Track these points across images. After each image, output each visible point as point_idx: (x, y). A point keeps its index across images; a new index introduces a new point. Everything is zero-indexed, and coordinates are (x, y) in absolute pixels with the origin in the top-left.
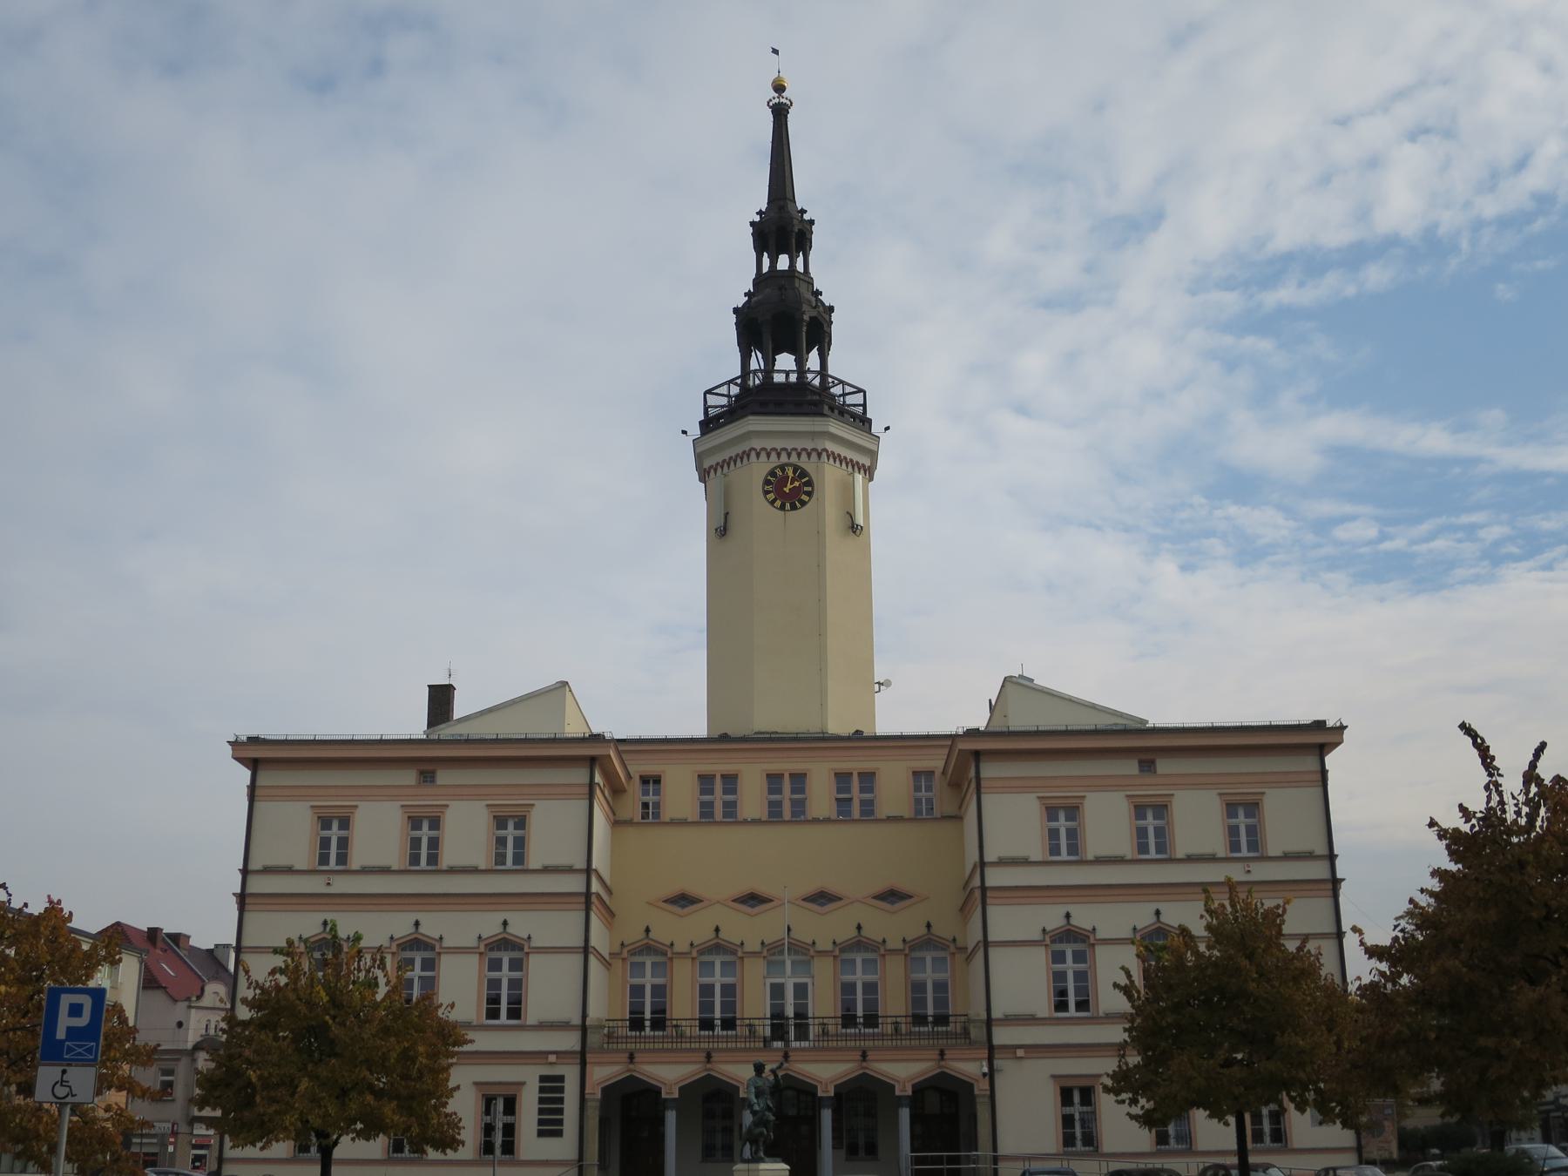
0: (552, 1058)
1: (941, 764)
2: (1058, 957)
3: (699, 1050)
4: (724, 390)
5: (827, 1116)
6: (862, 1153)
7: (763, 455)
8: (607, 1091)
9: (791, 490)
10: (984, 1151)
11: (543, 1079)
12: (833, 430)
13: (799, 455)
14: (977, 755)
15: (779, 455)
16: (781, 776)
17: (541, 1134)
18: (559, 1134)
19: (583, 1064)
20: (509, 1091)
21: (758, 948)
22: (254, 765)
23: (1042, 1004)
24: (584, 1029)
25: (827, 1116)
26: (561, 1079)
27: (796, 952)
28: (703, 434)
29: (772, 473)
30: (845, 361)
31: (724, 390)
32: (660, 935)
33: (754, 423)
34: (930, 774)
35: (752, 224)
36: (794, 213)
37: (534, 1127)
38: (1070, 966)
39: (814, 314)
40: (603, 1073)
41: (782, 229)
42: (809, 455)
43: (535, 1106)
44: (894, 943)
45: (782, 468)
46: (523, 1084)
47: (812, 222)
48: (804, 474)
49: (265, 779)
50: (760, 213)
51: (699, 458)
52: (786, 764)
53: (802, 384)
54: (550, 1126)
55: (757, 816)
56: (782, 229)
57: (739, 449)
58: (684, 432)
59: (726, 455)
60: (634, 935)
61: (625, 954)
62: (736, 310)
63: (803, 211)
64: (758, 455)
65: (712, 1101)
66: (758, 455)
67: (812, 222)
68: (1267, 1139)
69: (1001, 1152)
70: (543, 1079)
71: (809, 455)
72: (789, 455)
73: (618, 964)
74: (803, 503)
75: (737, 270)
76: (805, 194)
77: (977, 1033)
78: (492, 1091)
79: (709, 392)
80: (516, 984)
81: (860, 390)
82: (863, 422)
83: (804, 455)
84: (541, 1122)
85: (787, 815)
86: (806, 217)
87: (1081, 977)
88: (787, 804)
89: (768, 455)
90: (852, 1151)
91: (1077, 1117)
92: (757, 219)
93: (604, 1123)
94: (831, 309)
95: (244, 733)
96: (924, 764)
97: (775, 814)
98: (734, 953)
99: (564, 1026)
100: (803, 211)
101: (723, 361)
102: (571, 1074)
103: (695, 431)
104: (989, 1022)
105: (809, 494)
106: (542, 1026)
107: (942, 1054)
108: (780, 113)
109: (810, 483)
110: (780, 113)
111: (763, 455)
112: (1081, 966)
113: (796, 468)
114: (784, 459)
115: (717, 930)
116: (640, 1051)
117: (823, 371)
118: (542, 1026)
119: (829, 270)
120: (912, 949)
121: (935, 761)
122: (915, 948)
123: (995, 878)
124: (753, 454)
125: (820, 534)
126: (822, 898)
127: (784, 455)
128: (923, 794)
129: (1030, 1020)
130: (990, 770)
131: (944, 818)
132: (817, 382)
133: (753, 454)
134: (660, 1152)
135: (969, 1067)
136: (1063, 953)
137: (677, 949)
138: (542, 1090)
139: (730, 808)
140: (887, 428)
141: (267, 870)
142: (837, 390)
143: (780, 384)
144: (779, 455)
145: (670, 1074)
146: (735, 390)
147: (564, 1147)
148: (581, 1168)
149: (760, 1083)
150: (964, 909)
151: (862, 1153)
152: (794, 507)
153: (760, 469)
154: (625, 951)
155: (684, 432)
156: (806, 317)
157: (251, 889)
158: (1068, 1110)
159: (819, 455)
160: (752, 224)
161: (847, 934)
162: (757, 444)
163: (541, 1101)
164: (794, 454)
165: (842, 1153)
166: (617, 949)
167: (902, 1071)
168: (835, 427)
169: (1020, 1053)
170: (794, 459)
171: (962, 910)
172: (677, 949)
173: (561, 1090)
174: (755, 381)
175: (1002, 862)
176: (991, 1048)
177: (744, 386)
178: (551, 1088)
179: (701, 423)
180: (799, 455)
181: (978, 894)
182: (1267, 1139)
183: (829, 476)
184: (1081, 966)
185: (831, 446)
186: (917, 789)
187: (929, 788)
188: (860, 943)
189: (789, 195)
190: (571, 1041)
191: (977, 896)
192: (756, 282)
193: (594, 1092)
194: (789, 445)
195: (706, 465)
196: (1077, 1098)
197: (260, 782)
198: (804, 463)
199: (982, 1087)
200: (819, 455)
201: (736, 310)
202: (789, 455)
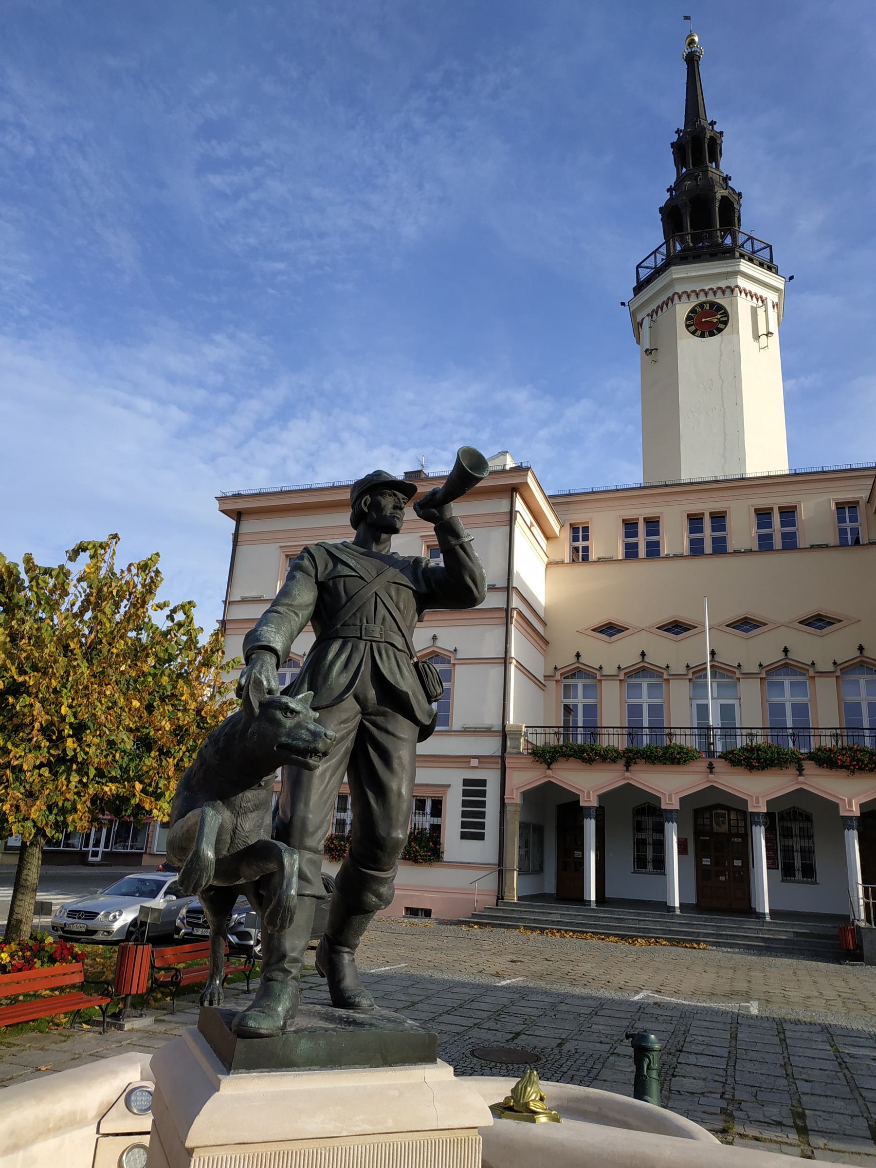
0: (474, 762)
1: (864, 495)
5: (590, 826)
7: (684, 297)
8: (526, 795)
11: (466, 782)
13: (715, 293)
15: (697, 295)
17: (464, 836)
18: (481, 837)
20: (436, 794)
21: (683, 671)
22: (238, 516)
25: (590, 826)
26: (483, 783)
27: (722, 676)
28: (635, 295)
29: (693, 311)
32: (590, 660)
33: (678, 272)
34: (853, 505)
37: (459, 830)
39: (725, 193)
40: (524, 778)
43: (460, 809)
45: (701, 305)
46: (449, 786)
49: (248, 526)
51: (633, 315)
54: (472, 830)
56: (696, 147)
57: (664, 298)
59: (659, 302)
60: (566, 660)
61: (558, 677)
64: (680, 297)
66: (680, 297)
67: (721, 133)
70: (466, 782)
73: (552, 685)
79: (638, 266)
83: (719, 293)
84: (464, 825)
86: (717, 128)
89: (689, 296)
90: (788, 872)
95: (230, 490)
96: (847, 495)
99: (487, 731)
100: (713, 123)
102: (492, 777)
106: (467, 731)
108: (692, 60)
110: (692, 60)
111: (684, 297)
113: (712, 304)
114: (702, 298)
115: (643, 654)
118: (467, 731)
122: (845, 670)
124: (676, 297)
128: (848, 525)
133: (676, 297)
137: (606, 672)
138: (465, 793)
141: (244, 601)
145: (588, 784)
147: (483, 851)
148: (501, 873)
151: (798, 875)
153: (682, 310)
154: (558, 674)
156: (718, 196)
157: (231, 616)
163: (465, 804)
166: (550, 672)
168: (745, 266)
170: (711, 298)
172: (606, 672)
173: (483, 794)
178: (474, 790)
180: (715, 293)
186: (841, 520)
187: (854, 519)
188: (786, 666)
190: (490, 746)
193: (514, 797)
195: (639, 320)
197: (242, 530)
198: (720, 300)
200: (732, 291)
202: (706, 294)
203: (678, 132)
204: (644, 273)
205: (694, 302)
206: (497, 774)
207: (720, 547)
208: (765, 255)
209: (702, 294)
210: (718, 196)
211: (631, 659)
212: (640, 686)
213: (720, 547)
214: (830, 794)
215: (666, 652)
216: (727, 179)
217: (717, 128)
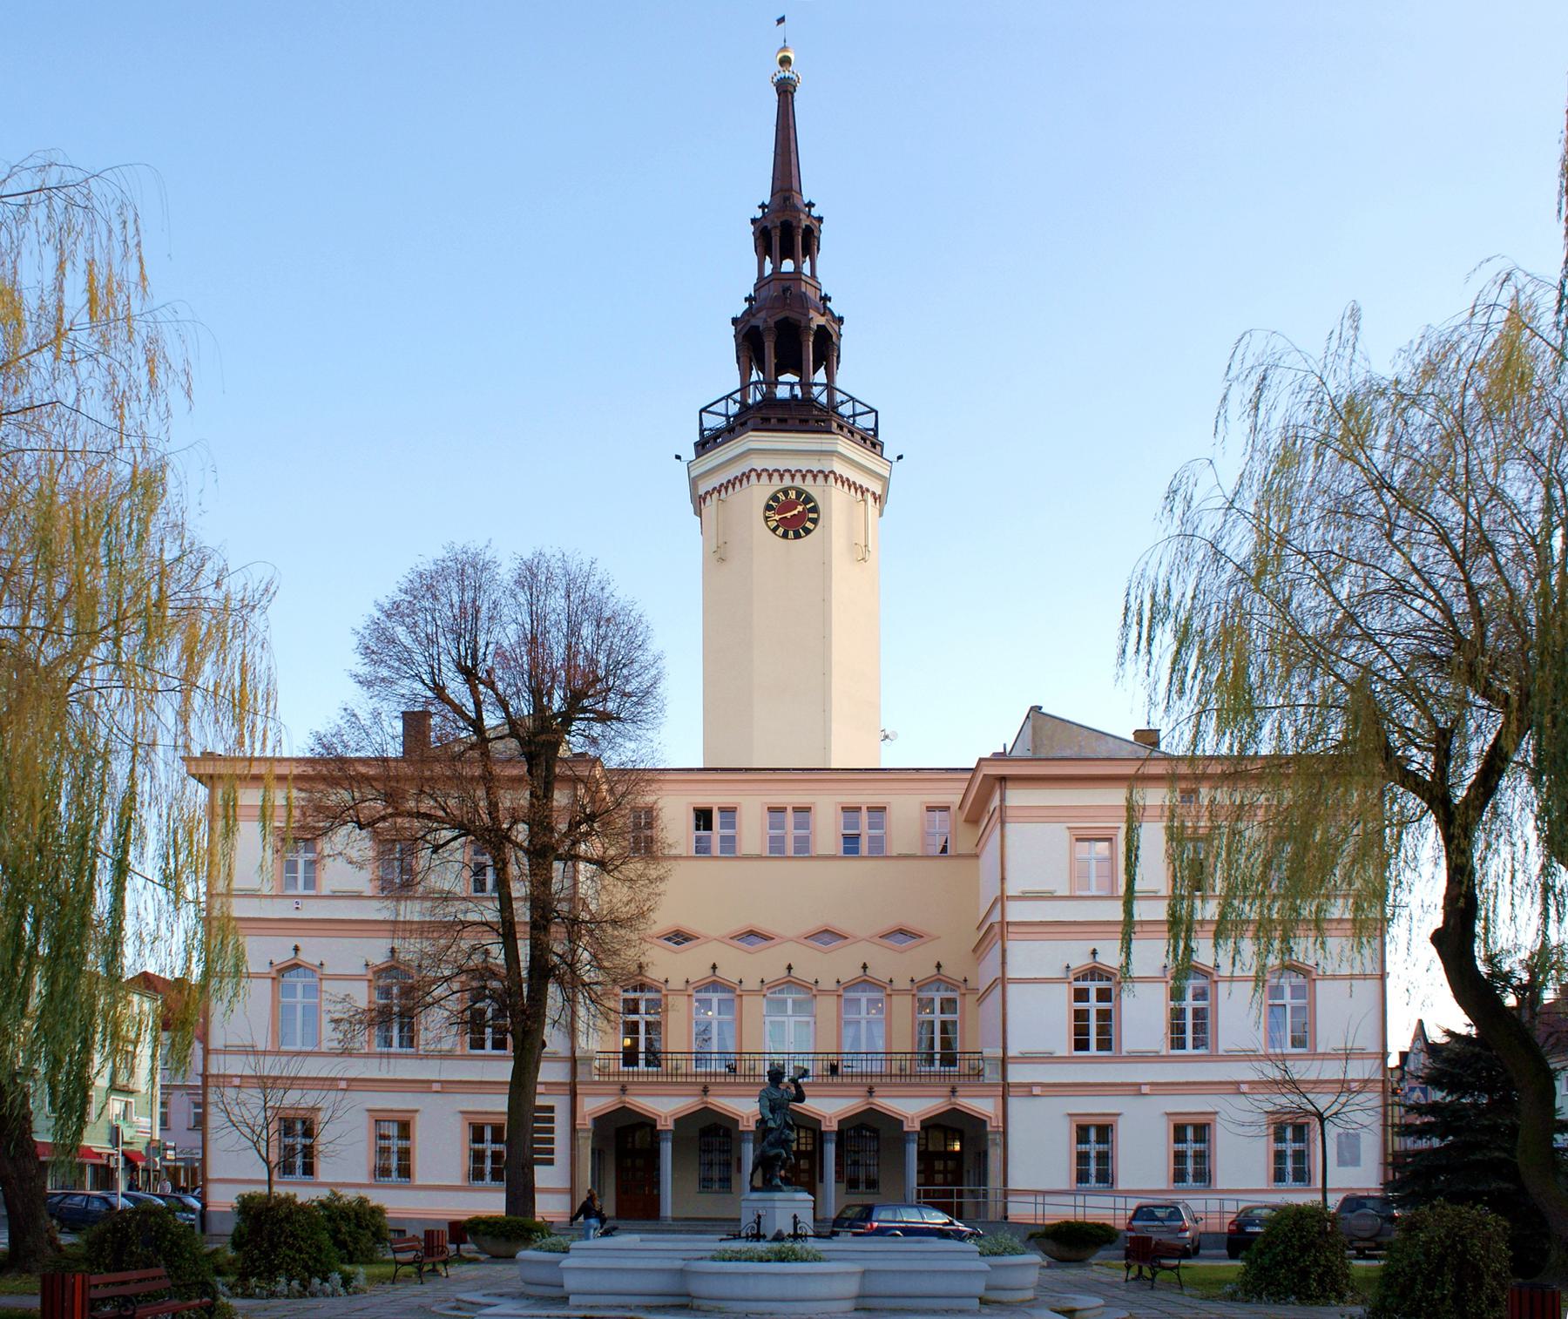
1: (957, 799)
2: (1081, 995)
3: (696, 1084)
4: (720, 408)
5: (830, 1150)
6: (862, 1188)
8: (601, 1121)
9: (794, 516)
10: (994, 1182)
12: (840, 449)
13: (804, 477)
14: (1003, 779)
15: (781, 477)
16: (783, 810)
19: (574, 1096)
23: (1062, 1042)
24: (574, 1060)
25: (830, 1150)
26: (551, 1109)
28: (698, 455)
29: (775, 498)
30: (857, 374)
31: (720, 408)
33: (754, 440)
35: (754, 221)
36: (800, 206)
38: (1093, 1005)
39: (821, 321)
40: (593, 1105)
41: (786, 230)
42: (815, 477)
44: (828, 983)
45: (785, 492)
47: (820, 219)
48: (809, 499)
50: (763, 206)
51: (694, 482)
52: (791, 797)
53: (808, 401)
55: (757, 852)
56: (786, 230)
57: (735, 471)
58: (678, 457)
62: (735, 321)
63: (810, 205)
64: (759, 476)
65: (709, 1135)
66: (759, 476)
67: (820, 219)
68: (1289, 1178)
69: (1011, 1186)
71: (815, 477)
72: (793, 477)
74: (808, 531)
75: (737, 273)
76: (813, 187)
77: (991, 1075)
78: (479, 1119)
80: (1104, 1015)
81: (873, 410)
82: (871, 441)
83: (809, 476)
85: (790, 851)
86: (815, 212)
87: (1104, 1015)
88: (790, 838)
89: (770, 476)
91: (1289, 1152)
92: (759, 214)
93: (597, 1154)
94: (841, 320)
97: (776, 848)
98: (658, 991)
100: (810, 205)
101: (719, 374)
103: (689, 454)
104: (1004, 1061)
105: (815, 521)
107: (953, 1091)
108: (785, 90)
109: (815, 509)
110: (785, 90)
112: (1104, 1005)
113: (799, 493)
114: (787, 482)
116: (633, 1083)
117: (830, 387)
119: (837, 272)
120: (920, 989)
121: (952, 795)
123: (1015, 912)
125: (825, 565)
126: (827, 935)
127: (787, 477)
129: (1049, 1058)
130: (1017, 797)
131: (959, 856)
132: (823, 399)
134: (656, 1183)
135: (983, 1106)
136: (1086, 991)
137: (896, 985)
139: (729, 843)
140: (900, 457)
142: (846, 410)
143: (783, 401)
144: (781, 477)
145: (665, 1107)
146: (734, 409)
149: (776, 1095)
150: (979, 949)
151: (862, 1188)
152: (797, 536)
153: (761, 492)
155: (678, 457)
158: (1083, 1147)
159: (826, 477)
160: (754, 221)
161: (851, 972)
162: (759, 463)
164: (787, 476)
165: (843, 1186)
167: (912, 1108)
168: (843, 445)
169: (1036, 1091)
170: (798, 482)
171: (974, 950)
174: (755, 396)
175: (1023, 897)
176: (1006, 1086)
177: (743, 403)
179: (696, 445)
180: (804, 477)
181: (997, 928)
182: (1289, 1178)
183: (836, 503)
184: (1104, 1005)
185: (839, 468)
189: (795, 186)
191: (993, 933)
192: (757, 288)
194: (793, 464)
195: (702, 492)
196: (1093, 1135)
198: (809, 486)
199: (994, 1123)
200: (826, 477)
201: (735, 321)
202: (793, 477)
203: (763, 206)
204: (713, 422)
205: (777, 484)
206: (567, 1099)
207: (803, 849)
208: (865, 422)
209: (787, 476)
210: (814, 326)
211: (701, 973)
212: (785, 1001)
213: (803, 849)
214: (935, 1312)
215: (739, 965)
216: (826, 299)
217: (815, 212)
